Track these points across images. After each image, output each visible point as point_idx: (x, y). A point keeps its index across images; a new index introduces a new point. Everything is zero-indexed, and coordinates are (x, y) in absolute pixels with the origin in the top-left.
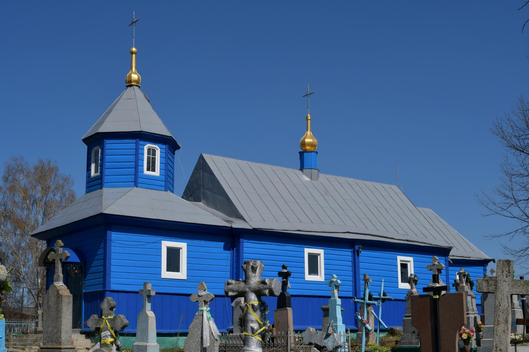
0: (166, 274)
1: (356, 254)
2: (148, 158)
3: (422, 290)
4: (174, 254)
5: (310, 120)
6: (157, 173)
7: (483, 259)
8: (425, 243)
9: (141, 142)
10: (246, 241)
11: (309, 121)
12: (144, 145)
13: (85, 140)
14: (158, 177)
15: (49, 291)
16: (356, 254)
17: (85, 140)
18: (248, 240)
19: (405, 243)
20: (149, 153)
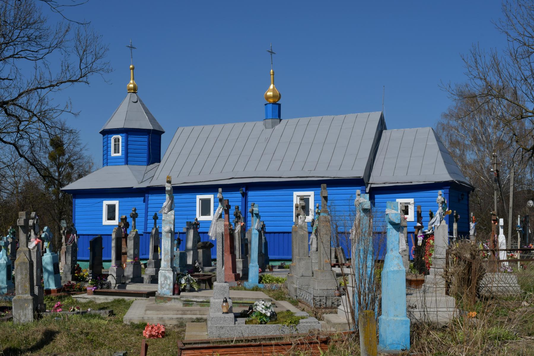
0: (106, 222)
1: (244, 195)
2: (115, 145)
3: (186, 224)
4: (111, 209)
5: (271, 75)
6: (119, 154)
7: (434, 182)
8: (323, 177)
9: (109, 136)
10: (150, 195)
11: (272, 74)
12: (111, 137)
13: (101, 133)
14: (120, 156)
15: (388, 256)
16: (244, 195)
17: (101, 133)
18: (151, 194)
19: (280, 181)
20: (115, 141)
